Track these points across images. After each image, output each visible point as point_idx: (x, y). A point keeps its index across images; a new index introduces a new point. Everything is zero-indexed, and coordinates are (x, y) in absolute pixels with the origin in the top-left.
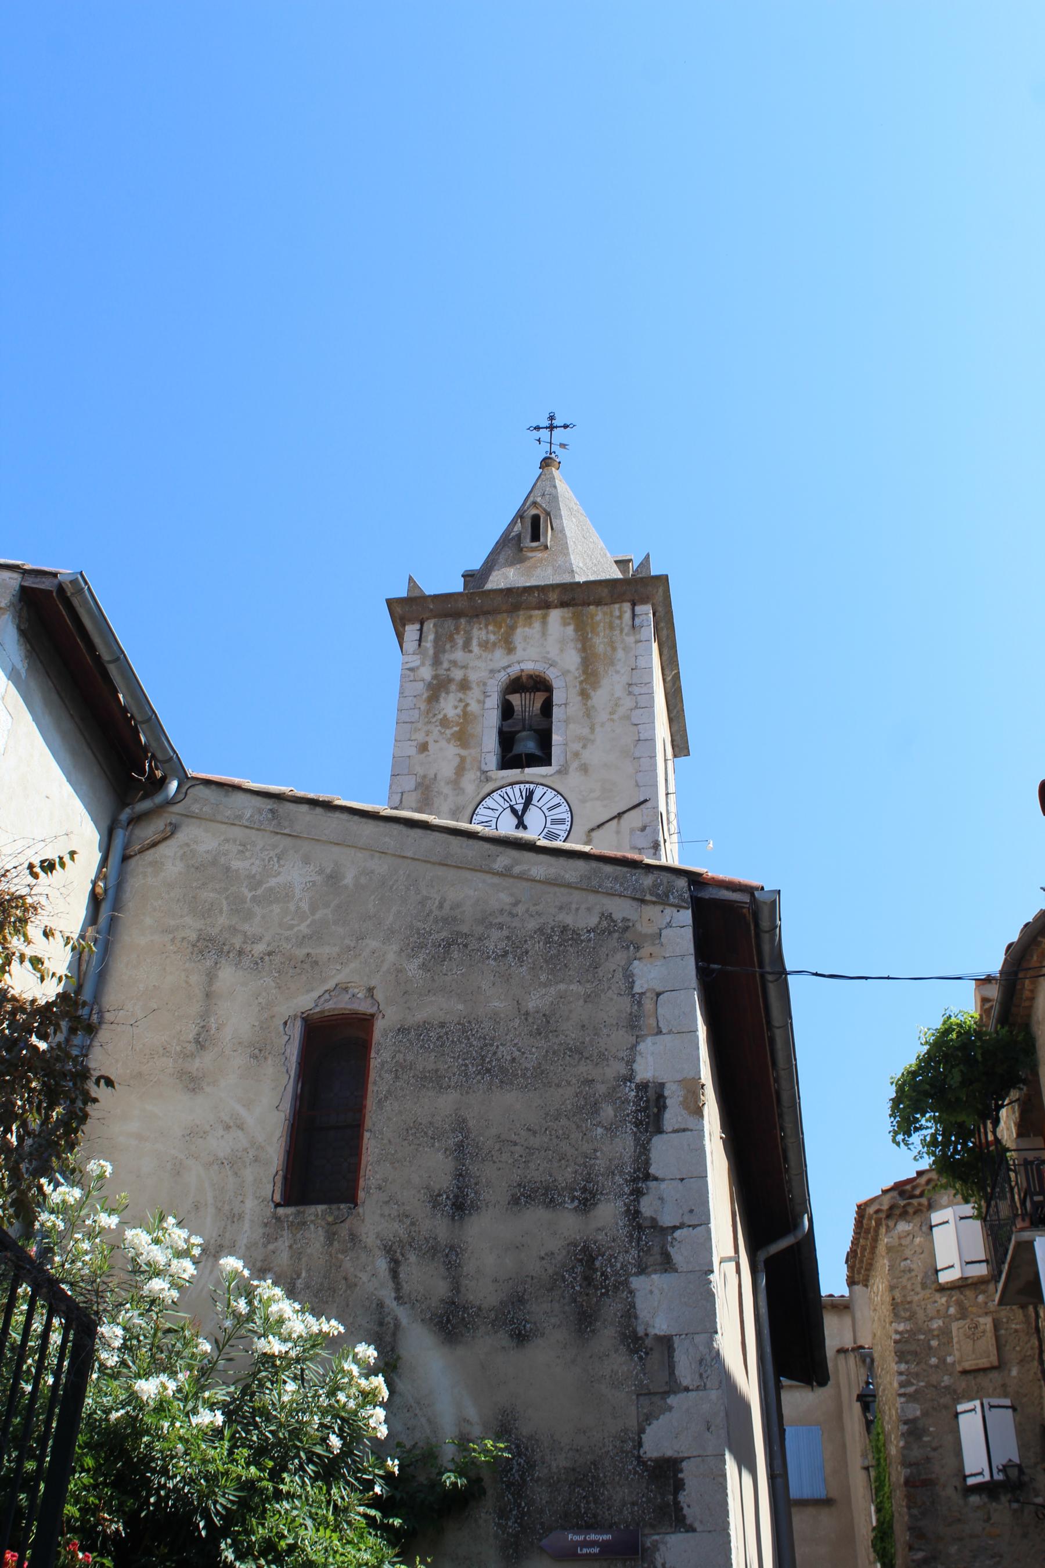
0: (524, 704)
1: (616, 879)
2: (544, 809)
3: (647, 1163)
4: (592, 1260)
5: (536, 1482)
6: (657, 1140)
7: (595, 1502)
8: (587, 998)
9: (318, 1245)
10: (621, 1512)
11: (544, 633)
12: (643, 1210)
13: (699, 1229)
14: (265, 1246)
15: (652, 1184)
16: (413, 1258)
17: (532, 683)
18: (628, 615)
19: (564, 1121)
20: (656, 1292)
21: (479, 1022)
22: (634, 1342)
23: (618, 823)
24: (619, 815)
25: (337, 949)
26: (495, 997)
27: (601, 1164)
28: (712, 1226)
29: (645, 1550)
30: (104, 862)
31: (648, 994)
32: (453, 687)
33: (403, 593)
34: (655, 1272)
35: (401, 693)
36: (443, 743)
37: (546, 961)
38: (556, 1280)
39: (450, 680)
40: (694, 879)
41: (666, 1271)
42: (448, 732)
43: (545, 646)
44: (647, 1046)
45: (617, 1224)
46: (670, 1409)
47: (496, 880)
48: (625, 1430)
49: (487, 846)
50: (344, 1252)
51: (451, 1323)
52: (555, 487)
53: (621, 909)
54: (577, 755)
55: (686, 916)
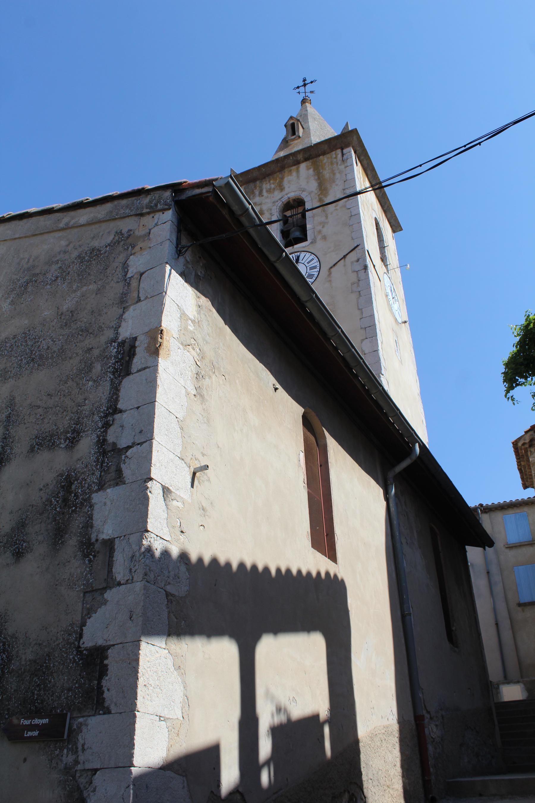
2: (306, 263)
3: (117, 401)
5: (10, 673)
8: (98, 292)
11: (298, 177)
12: (108, 438)
13: (144, 445)
18: (340, 155)
19: (70, 383)
20: (109, 503)
23: (345, 261)
24: (344, 257)
31: (135, 276)
38: (46, 505)
40: (176, 188)
41: (117, 484)
44: (131, 313)
45: (90, 453)
46: (105, 602)
47: (60, 234)
52: (307, 110)
53: (126, 225)
54: (320, 232)
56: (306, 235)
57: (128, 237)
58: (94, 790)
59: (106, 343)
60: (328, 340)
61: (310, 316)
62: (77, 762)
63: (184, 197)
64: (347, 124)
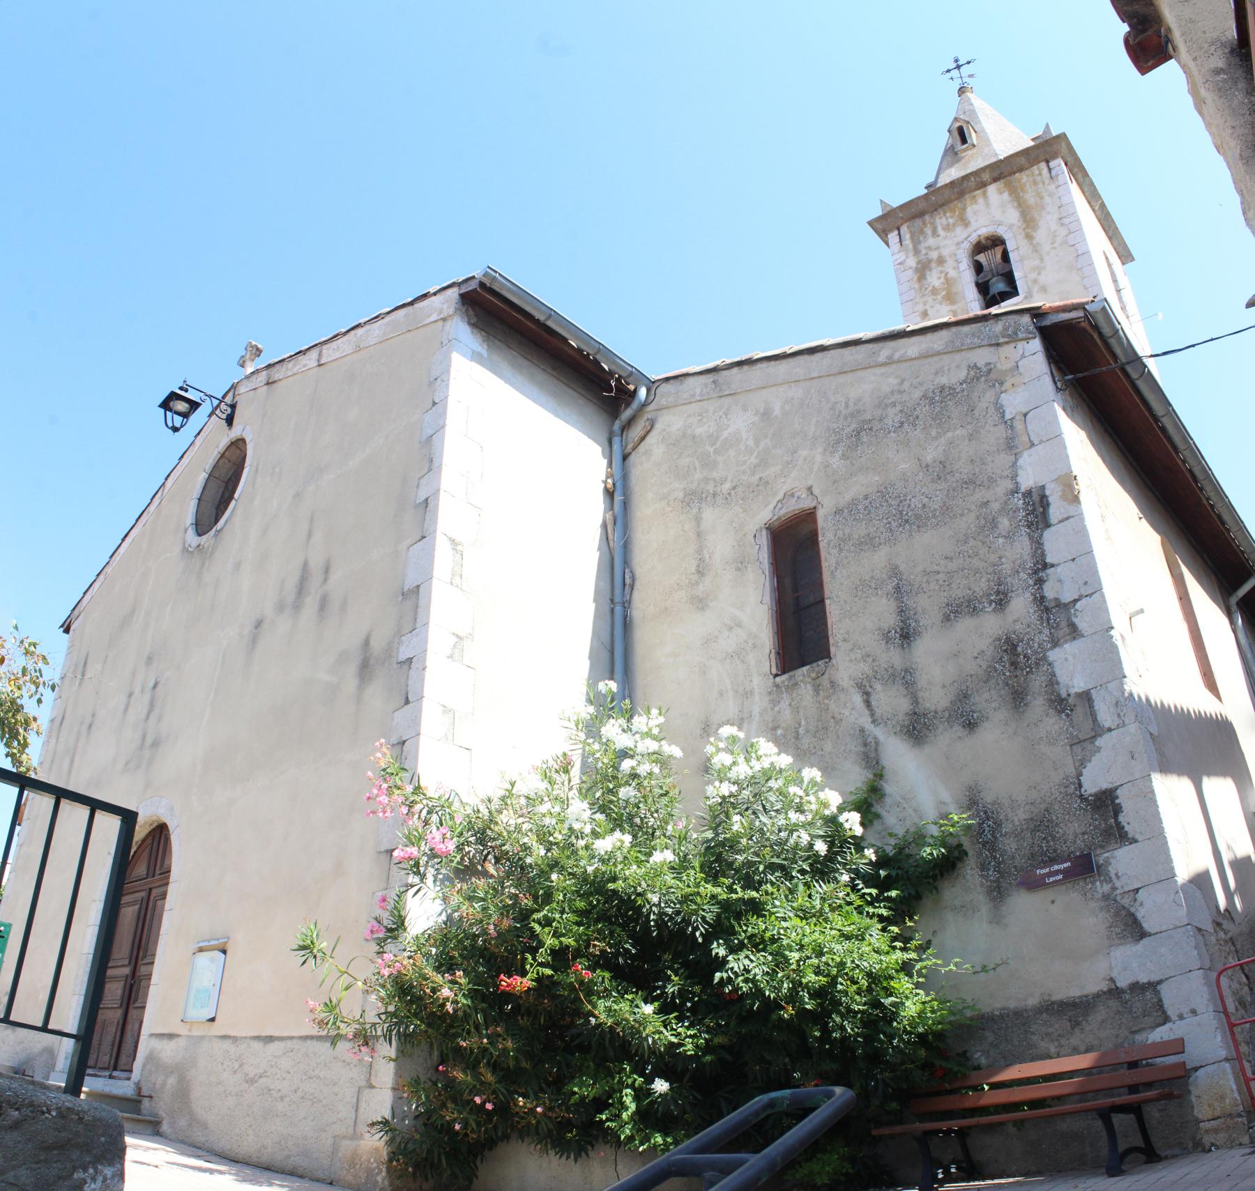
0: (989, 259)
1: (973, 335)
3: (1043, 554)
4: (1015, 647)
6: (1048, 534)
7: (1053, 840)
8: (971, 437)
9: (809, 698)
10: (1075, 842)
11: (988, 205)
12: (1046, 594)
14: (772, 709)
15: (1050, 571)
16: (878, 687)
17: (990, 243)
18: (1045, 171)
19: (972, 542)
20: (1070, 658)
21: (893, 485)
22: (1060, 704)
25: (780, 467)
26: (899, 461)
27: (1007, 567)
28: (1105, 590)
29: (1099, 867)
30: (610, 464)
32: (933, 265)
33: (879, 212)
34: (1066, 642)
35: (898, 282)
36: (937, 306)
37: (934, 419)
39: (930, 261)
41: (1075, 638)
42: (939, 297)
43: (991, 212)
44: (1026, 460)
46: (1099, 749)
47: (883, 370)
48: (1066, 778)
49: (870, 346)
50: (828, 697)
51: (917, 729)
53: (982, 357)
54: (1035, 281)
55: (1036, 344)
56: (1015, 288)
57: (990, 371)
58: (1141, 904)
59: (1006, 494)
60: (565, 340)
61: (1164, 430)
62: (1114, 889)
63: (1047, 322)
64: (1047, 126)
